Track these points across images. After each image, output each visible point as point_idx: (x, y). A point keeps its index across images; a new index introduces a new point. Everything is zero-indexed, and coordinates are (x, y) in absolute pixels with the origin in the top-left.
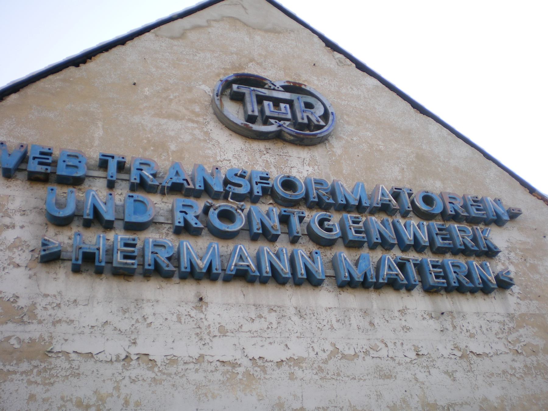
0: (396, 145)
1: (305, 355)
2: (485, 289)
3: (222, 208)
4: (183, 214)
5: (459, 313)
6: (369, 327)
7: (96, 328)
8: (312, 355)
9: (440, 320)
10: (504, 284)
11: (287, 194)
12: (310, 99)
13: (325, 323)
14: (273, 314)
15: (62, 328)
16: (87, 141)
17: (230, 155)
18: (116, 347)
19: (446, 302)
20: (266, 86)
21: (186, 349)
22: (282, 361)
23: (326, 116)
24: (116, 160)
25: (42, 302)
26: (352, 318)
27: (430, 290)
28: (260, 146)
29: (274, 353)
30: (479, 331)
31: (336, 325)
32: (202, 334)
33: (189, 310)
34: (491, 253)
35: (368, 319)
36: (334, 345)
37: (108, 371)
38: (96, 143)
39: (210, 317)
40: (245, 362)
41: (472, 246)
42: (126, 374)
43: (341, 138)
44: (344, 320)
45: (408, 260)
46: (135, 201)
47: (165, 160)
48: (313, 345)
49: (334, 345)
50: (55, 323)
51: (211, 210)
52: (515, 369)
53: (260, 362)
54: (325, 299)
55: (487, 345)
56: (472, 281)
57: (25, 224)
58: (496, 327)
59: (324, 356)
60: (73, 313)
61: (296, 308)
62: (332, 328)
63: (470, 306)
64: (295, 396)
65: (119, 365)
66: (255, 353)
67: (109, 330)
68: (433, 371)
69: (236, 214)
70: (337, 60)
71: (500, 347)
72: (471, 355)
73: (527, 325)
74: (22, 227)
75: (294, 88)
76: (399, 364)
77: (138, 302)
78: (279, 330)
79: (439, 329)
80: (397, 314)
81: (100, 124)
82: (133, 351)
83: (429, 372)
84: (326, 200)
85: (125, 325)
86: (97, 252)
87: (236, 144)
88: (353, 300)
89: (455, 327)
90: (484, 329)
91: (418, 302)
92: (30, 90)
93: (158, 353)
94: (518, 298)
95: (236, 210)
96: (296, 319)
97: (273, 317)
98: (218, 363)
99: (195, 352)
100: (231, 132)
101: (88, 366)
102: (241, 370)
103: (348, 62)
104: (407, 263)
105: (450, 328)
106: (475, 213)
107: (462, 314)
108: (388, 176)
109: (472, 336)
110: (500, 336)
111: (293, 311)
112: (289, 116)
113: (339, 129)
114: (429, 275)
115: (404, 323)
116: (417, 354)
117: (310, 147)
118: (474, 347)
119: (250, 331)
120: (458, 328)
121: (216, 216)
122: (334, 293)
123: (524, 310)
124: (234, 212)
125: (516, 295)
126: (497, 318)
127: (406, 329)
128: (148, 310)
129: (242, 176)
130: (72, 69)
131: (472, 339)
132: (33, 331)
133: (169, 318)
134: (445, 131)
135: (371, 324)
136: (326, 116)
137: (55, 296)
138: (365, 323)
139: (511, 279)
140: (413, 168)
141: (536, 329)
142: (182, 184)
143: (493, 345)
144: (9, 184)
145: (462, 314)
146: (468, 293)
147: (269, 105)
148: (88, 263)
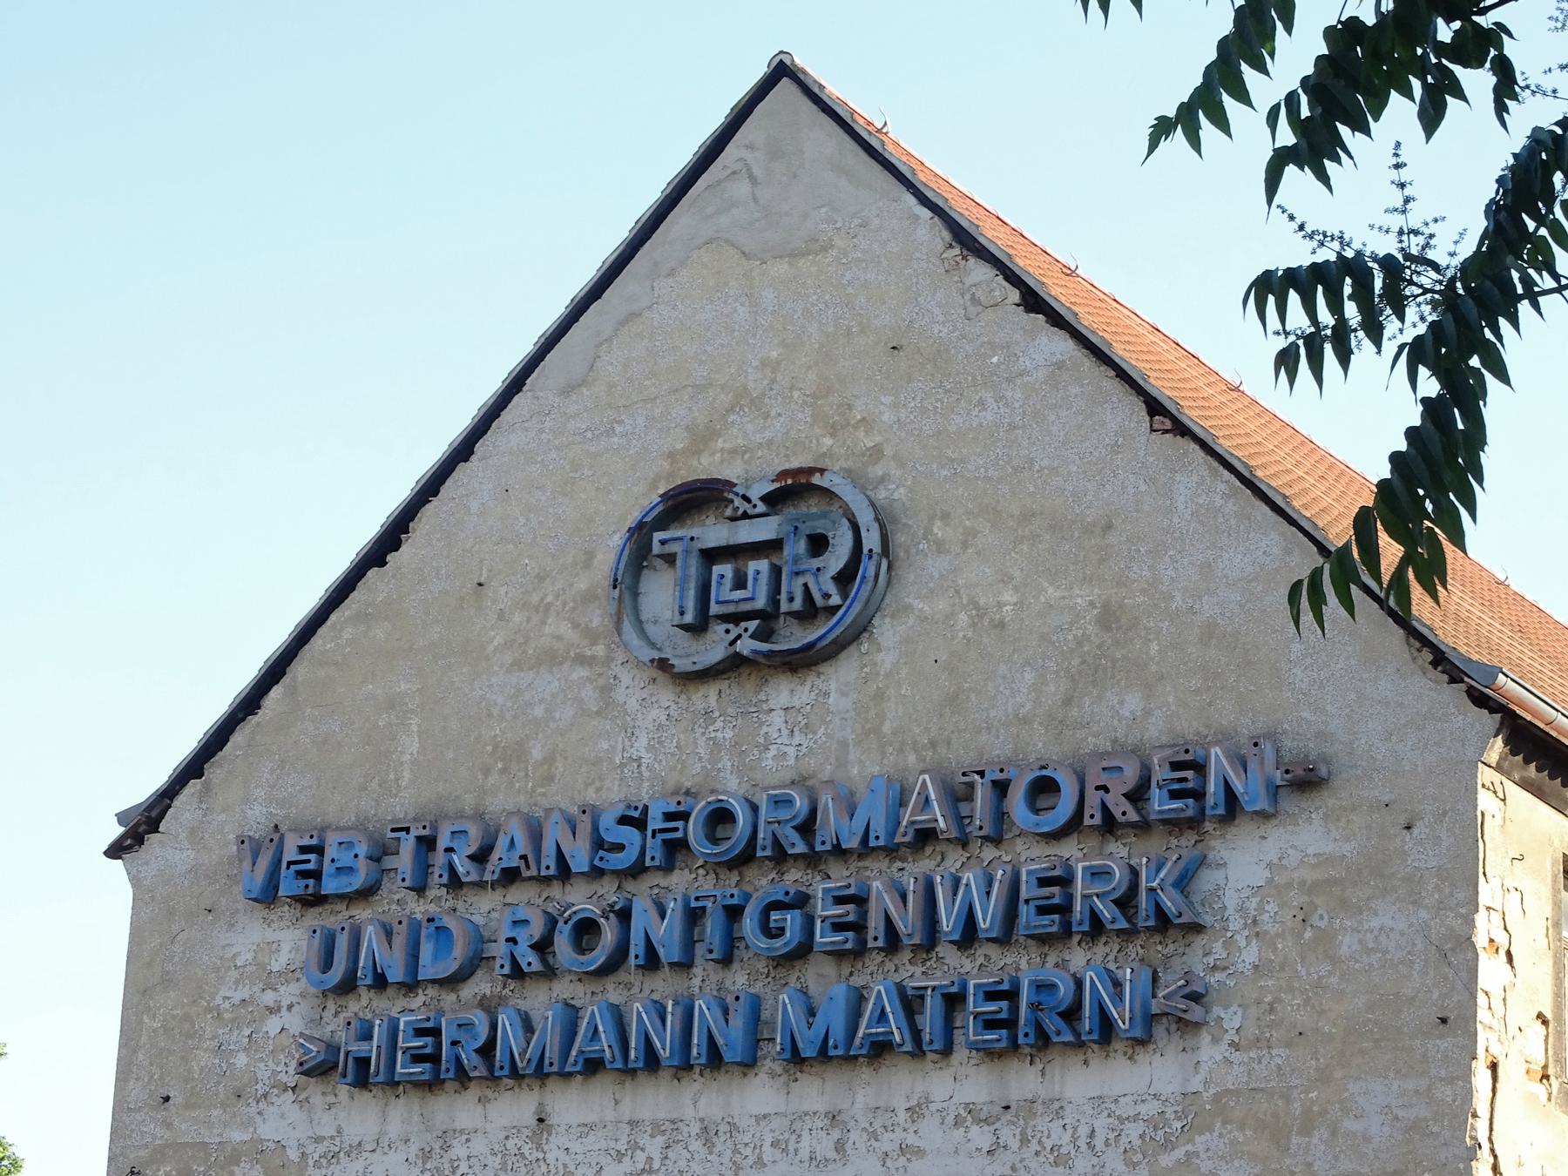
0: (1050, 590)
3: (575, 918)
6: (832, 1155)
9: (997, 1125)
17: (655, 744)
19: (1023, 1080)
26: (805, 1134)
30: (1084, 1147)
31: (768, 1153)
39: (551, 1158)
43: (908, 608)
44: (787, 1142)
47: (519, 791)
54: (759, 1097)
58: (1133, 1132)
73: (1224, 1123)
74: (290, 1007)
77: (445, 1138)
80: (902, 1116)
81: (414, 722)
84: (807, 841)
88: (815, 1093)
89: (1024, 1141)
90: (1099, 1142)
91: (963, 1083)
92: (299, 670)
94: (1232, 1044)
96: (696, 1145)
97: (654, 1146)
105: (1014, 1144)
111: (695, 1128)
113: (912, 577)
115: (911, 1139)
117: (824, 668)
120: (1034, 1146)
123: (1234, 1078)
129: (639, 823)
130: (372, 573)
133: (490, 1163)
135: (840, 1146)
137: (332, 1138)
138: (826, 1148)
141: (1249, 1133)
144: (1313, 748)
145: (1056, 1105)
147: (663, 542)
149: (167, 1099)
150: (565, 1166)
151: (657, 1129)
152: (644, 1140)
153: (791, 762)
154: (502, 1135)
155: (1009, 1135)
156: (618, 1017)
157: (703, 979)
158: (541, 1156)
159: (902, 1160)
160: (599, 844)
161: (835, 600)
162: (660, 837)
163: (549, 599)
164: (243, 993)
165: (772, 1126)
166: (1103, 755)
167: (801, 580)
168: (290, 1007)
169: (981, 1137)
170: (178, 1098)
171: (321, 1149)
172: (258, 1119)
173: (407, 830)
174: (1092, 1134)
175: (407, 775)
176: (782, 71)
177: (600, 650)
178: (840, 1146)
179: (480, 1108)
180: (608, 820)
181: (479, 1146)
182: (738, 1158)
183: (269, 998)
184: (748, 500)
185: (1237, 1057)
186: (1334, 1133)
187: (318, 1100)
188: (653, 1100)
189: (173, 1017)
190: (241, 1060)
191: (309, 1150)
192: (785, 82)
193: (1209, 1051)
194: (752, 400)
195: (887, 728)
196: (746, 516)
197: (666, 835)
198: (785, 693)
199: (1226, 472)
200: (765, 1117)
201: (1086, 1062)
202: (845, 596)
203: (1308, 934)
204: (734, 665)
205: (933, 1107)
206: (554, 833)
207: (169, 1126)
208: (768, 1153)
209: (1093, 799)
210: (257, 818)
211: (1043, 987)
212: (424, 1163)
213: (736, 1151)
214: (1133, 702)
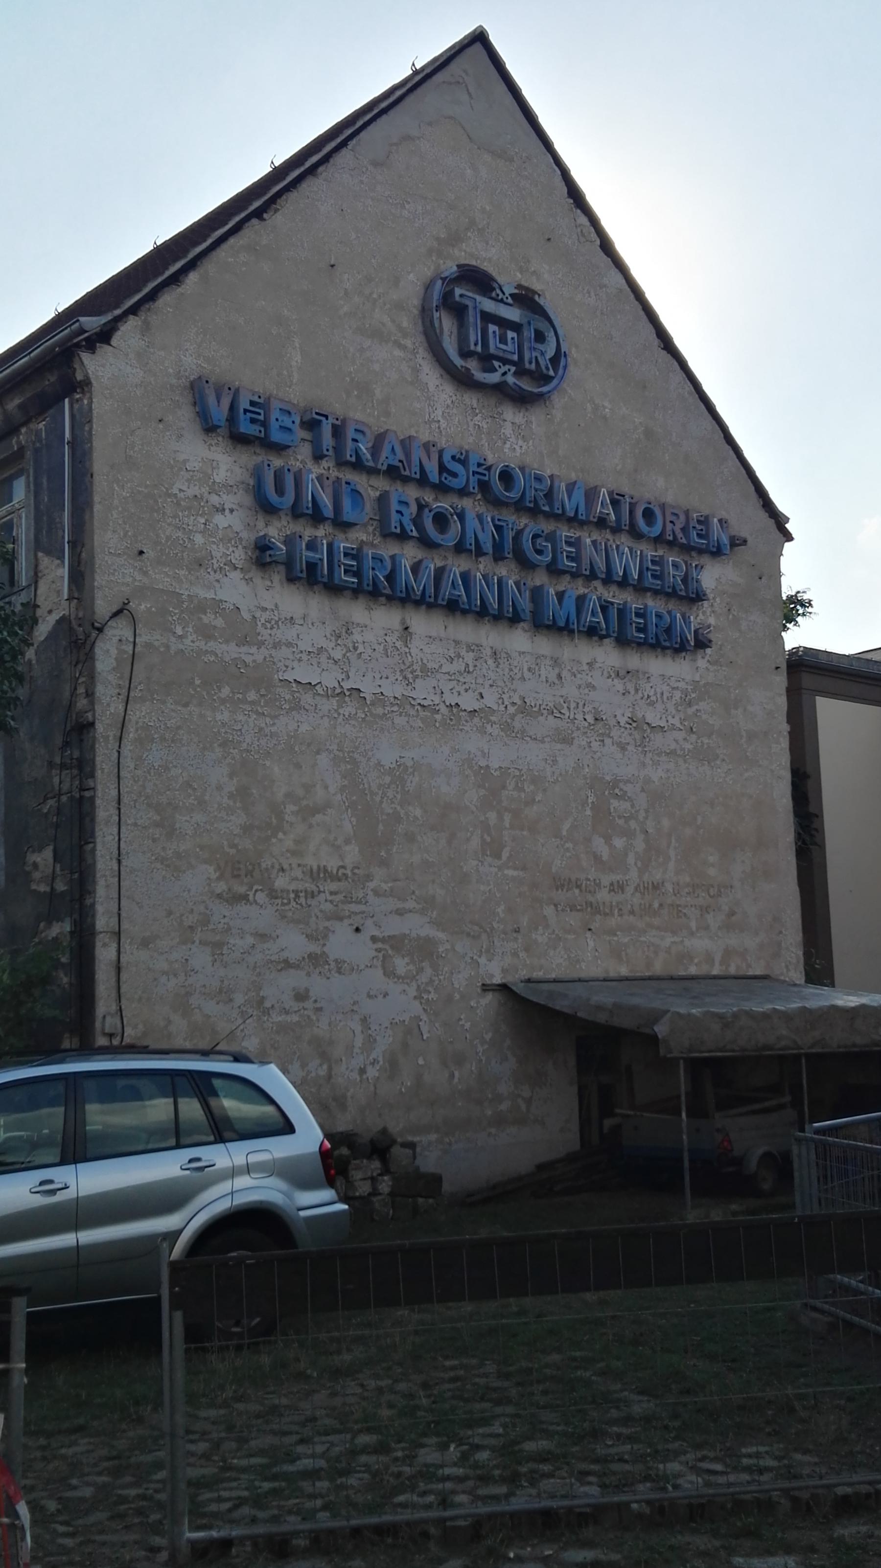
1: (495, 707)
2: (680, 648)
4: (399, 515)
5: (645, 673)
6: (556, 681)
7: (312, 655)
8: (502, 708)
10: (702, 644)
11: (497, 486)
12: (543, 325)
13: (516, 671)
14: (471, 653)
15: (285, 652)
16: (285, 372)
18: (330, 680)
19: (634, 660)
20: (494, 295)
21: (393, 689)
22: (475, 711)
23: (555, 360)
24: (331, 420)
25: (263, 617)
27: (623, 642)
28: (471, 399)
29: (468, 702)
31: (527, 675)
32: (410, 674)
33: (394, 641)
34: (697, 597)
35: (557, 671)
36: (523, 699)
37: (327, 705)
38: (296, 377)
39: (414, 651)
40: (443, 709)
41: (681, 590)
42: (341, 711)
45: (612, 604)
46: (352, 490)
48: (503, 696)
49: (523, 699)
50: (276, 645)
51: (426, 510)
52: (684, 749)
53: (455, 710)
55: (664, 716)
56: (670, 639)
57: (234, 507)
58: (678, 695)
59: (512, 710)
60: (289, 633)
61: (492, 648)
62: (523, 679)
63: (660, 667)
64: (482, 751)
65: (334, 702)
66: (451, 699)
67: (323, 658)
68: (608, 741)
69: (452, 521)
70: (579, 230)
71: (676, 722)
72: (645, 727)
75: (526, 299)
76: (578, 729)
78: (475, 674)
79: (622, 691)
80: (585, 667)
82: (347, 685)
83: (603, 741)
84: (541, 503)
85: (338, 654)
86: (319, 562)
87: (443, 393)
88: (545, 645)
89: (637, 690)
91: (607, 655)
93: (368, 689)
94: (708, 661)
95: (452, 515)
96: (490, 662)
97: (469, 657)
98: (419, 708)
99: (399, 690)
100: (443, 373)
101: (307, 699)
102: (438, 717)
103: (594, 235)
104: (611, 607)
105: (633, 692)
106: (695, 542)
107: (647, 675)
108: (611, 468)
109: (652, 704)
110: (680, 708)
111: (488, 652)
112: (515, 358)
114: (629, 626)
116: (596, 719)
118: (653, 717)
119: (448, 673)
120: (640, 695)
121: (430, 519)
122: (529, 634)
124: (450, 517)
125: (707, 657)
126: (681, 685)
127: (591, 687)
128: (357, 637)
129: (464, 462)
131: (651, 708)
132: (253, 655)
134: (689, 386)
135: (559, 677)
136: (555, 360)
138: (553, 677)
139: (710, 641)
140: (637, 451)
142: (398, 467)
143: (670, 718)
146: (659, 650)
148: (310, 576)
149: (141, 553)
150: (422, 660)
151: (469, 649)
152: (463, 653)
153: (518, 454)
154: (383, 632)
155: (631, 687)
156: (466, 577)
157: (484, 565)
158: (407, 650)
159: (586, 691)
160: (442, 468)
161: (551, 373)
162: (477, 476)
163: (375, 296)
164: (194, 490)
165: (526, 659)
166: (674, 507)
167: (534, 354)
168: (232, 511)
169: (619, 685)
170: (150, 553)
171: (266, 616)
172: (216, 584)
173: (327, 417)
174: (662, 694)
175: (296, 375)
176: (479, 38)
177: (408, 343)
178: (559, 677)
179: (367, 612)
180: (447, 458)
181: (369, 636)
182: (511, 673)
183: (215, 499)
184: (504, 294)
185: (712, 668)
186: (745, 710)
187: (258, 581)
188: (465, 630)
189: (139, 492)
190: (199, 539)
191: (258, 615)
192: (478, 46)
193: (702, 663)
194: (479, 229)
195: (560, 452)
196: (502, 301)
197: (447, 474)
198: (511, 414)
199: (689, 383)
200: (524, 653)
201: (657, 657)
202: (556, 370)
203: (731, 617)
204: (500, 390)
205: (598, 665)
206: (418, 454)
207: (145, 573)
208: (527, 675)
209: (669, 526)
210: (192, 363)
211: (659, 616)
212: (337, 640)
213: (511, 670)
214: (661, 483)
